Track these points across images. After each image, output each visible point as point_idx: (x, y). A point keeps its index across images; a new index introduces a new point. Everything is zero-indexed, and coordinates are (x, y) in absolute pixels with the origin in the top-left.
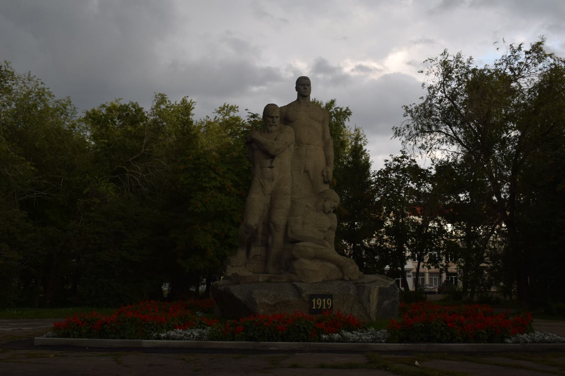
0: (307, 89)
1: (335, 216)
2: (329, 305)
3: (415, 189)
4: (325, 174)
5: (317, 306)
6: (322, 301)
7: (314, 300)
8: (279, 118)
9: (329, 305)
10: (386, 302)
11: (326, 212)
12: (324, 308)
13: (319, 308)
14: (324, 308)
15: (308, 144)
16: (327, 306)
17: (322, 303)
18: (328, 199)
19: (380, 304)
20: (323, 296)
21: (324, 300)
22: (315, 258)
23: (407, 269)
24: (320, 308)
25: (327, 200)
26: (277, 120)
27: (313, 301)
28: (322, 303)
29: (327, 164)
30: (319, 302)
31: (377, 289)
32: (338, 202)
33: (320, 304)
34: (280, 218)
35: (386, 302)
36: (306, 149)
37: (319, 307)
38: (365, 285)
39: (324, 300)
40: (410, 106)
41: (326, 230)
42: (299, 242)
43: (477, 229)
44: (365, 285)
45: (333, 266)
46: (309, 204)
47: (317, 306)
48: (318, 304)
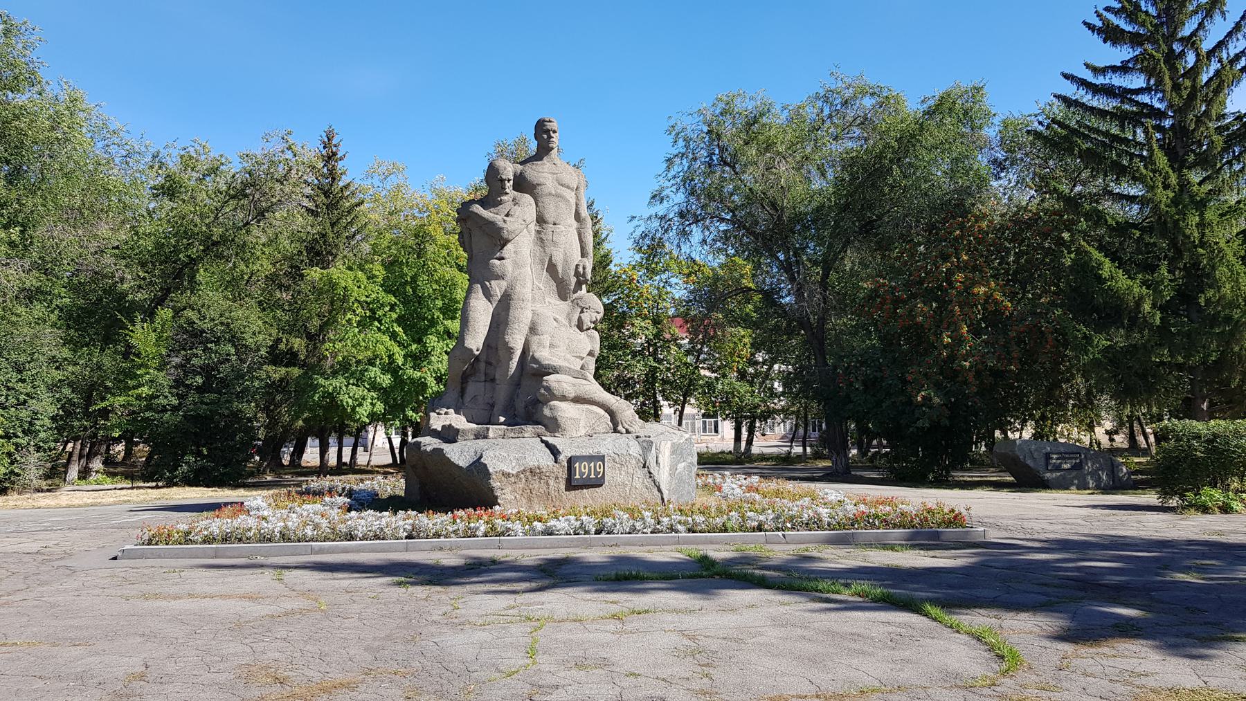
1: (596, 334)
4: (581, 270)
5: (581, 474)
7: (577, 465)
8: (511, 182)
10: (681, 466)
11: (585, 328)
12: (593, 476)
14: (593, 476)
15: (555, 224)
16: (597, 473)
17: (590, 468)
19: (673, 468)
20: (590, 458)
21: (592, 464)
22: (578, 400)
23: (559, 414)
25: (585, 310)
26: (509, 185)
28: (590, 468)
29: (584, 254)
34: (516, 341)
35: (681, 466)
38: (651, 439)
39: (592, 464)
40: (20, 384)
41: (585, 356)
42: (550, 374)
43: (120, 447)
44: (651, 439)
45: (602, 412)
48: (598, 470)
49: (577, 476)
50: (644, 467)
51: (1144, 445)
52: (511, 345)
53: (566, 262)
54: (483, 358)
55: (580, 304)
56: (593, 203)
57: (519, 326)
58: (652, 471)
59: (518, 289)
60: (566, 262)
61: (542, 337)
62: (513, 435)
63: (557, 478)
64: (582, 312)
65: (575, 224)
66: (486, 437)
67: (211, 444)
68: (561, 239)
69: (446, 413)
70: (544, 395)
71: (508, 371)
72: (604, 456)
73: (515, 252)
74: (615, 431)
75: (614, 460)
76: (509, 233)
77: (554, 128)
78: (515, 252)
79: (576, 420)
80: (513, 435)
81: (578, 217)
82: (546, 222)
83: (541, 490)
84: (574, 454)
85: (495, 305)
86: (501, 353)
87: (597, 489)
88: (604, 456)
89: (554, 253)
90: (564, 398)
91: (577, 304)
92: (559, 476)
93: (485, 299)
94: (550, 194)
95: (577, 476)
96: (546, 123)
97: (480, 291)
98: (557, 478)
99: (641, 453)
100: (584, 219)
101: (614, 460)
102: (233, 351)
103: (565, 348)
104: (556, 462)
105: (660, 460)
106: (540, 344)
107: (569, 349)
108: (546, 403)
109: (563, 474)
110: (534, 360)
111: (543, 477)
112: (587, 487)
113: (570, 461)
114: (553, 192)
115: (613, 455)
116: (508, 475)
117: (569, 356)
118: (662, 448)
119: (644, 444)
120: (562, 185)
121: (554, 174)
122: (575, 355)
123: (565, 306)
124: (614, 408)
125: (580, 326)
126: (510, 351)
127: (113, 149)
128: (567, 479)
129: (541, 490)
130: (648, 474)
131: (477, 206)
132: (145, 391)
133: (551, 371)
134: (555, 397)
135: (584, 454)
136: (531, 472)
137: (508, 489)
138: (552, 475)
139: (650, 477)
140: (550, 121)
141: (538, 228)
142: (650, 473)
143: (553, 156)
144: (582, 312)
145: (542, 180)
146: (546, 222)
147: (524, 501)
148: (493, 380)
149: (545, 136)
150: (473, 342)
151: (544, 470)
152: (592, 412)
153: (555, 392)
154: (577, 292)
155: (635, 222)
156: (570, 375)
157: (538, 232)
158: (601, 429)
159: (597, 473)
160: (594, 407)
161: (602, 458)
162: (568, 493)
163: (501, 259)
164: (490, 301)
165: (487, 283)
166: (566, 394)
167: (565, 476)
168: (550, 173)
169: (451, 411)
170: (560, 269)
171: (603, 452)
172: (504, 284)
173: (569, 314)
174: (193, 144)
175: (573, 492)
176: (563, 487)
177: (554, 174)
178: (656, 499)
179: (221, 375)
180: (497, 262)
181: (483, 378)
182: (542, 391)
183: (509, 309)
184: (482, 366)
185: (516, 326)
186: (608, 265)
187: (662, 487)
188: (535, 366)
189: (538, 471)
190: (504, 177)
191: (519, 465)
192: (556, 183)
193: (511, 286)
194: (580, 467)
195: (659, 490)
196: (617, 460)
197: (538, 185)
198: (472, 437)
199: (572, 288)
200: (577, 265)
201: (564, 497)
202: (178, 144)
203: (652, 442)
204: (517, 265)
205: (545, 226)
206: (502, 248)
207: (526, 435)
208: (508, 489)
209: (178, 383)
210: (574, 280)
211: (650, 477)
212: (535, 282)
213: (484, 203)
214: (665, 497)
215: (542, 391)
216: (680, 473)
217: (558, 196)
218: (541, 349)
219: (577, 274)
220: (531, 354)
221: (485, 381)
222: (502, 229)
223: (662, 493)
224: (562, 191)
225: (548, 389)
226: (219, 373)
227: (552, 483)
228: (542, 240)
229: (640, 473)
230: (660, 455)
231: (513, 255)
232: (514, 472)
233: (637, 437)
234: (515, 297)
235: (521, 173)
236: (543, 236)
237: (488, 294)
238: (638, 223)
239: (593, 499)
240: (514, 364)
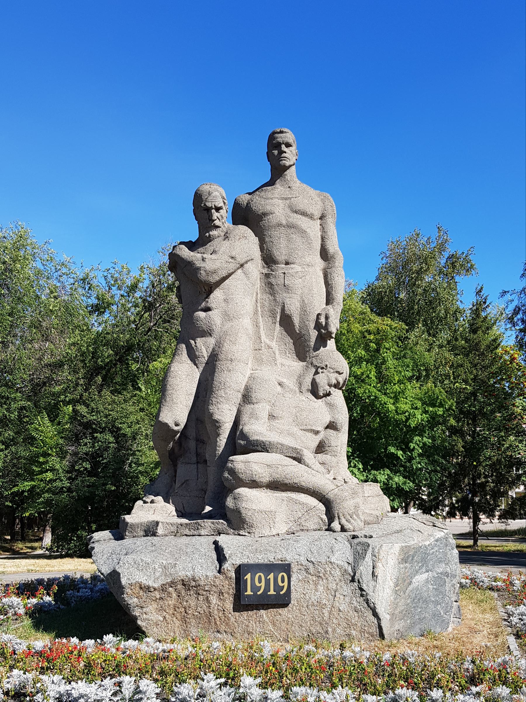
0: (285, 152)
2: (284, 586)
3: (208, 232)
4: (323, 320)
5: (255, 589)
6: (266, 579)
7: (248, 576)
9: (284, 586)
12: (272, 592)
13: (282, 593)
14: (272, 592)
15: (287, 263)
16: (278, 588)
17: (268, 582)
18: (322, 368)
21: (271, 576)
23: (243, 505)
24: (260, 594)
25: (320, 370)
27: (245, 578)
28: (268, 582)
29: (329, 300)
30: (260, 582)
31: (397, 547)
32: (345, 374)
33: (263, 584)
35: (420, 579)
36: (284, 273)
37: (259, 591)
39: (271, 576)
46: (285, 380)
47: (255, 589)
48: (281, 584)
49: (249, 592)
50: (353, 580)
51: (206, 287)
52: (216, 417)
53: (304, 311)
54: (192, 433)
55: (315, 363)
56: (482, 288)
57: (226, 393)
58: (365, 587)
59: (227, 346)
60: (304, 311)
61: (256, 406)
62: (187, 532)
63: (221, 593)
64: (317, 373)
65: (320, 264)
66: (154, 534)
67: (100, 521)
68: (295, 282)
69: (152, 502)
70: (227, 479)
71: (216, 450)
72: (289, 565)
73: (226, 300)
74: (329, 529)
75: (307, 570)
76: (207, 274)
77: (286, 140)
78: (226, 300)
79: (270, 514)
80: (187, 532)
81: (325, 254)
82: (275, 262)
83: (199, 609)
84: (245, 561)
85: (201, 369)
86: (209, 427)
87: (280, 610)
88: (289, 565)
89: (287, 301)
90: (254, 484)
91: (312, 364)
92: (225, 589)
93: (189, 362)
94: (280, 225)
95: (249, 592)
96: (277, 135)
97: (185, 352)
98: (221, 593)
99: (351, 560)
100: (333, 257)
101: (307, 570)
102: (112, 439)
103: (291, 420)
104: (219, 572)
105: (379, 571)
106: (253, 415)
107: (296, 421)
108: (230, 490)
109: (229, 588)
110: (244, 436)
111: (201, 592)
112: (266, 606)
113: (240, 570)
114: (284, 222)
115: (305, 563)
116: (147, 589)
117: (295, 429)
118: (382, 554)
119: (358, 548)
120: (296, 212)
121: (286, 199)
122: (304, 427)
123: (298, 365)
124: (331, 496)
125: (314, 391)
126: (216, 425)
127: (64, 278)
128: (235, 595)
129: (199, 609)
130: (358, 591)
131: (184, 246)
132: (49, 475)
133: (259, 448)
134: (242, 483)
135: (261, 562)
136: (184, 585)
137: (151, 608)
138: (214, 589)
139: (362, 595)
140: (281, 132)
141: (265, 271)
142: (361, 589)
143: (288, 177)
144: (317, 373)
145: (268, 208)
146: (275, 262)
147: (178, 623)
148: (205, 461)
149: (276, 152)
150: (170, 414)
151: (202, 583)
152: (296, 502)
153: (241, 476)
154: (318, 349)
155: (508, 297)
156: (282, 453)
157: (267, 276)
158: (311, 524)
159: (278, 588)
160: (303, 495)
161: (286, 568)
162: (237, 614)
163: (207, 309)
164: (195, 364)
165: (192, 342)
166: (257, 478)
167: (232, 591)
168: (282, 199)
169: (160, 498)
170: (296, 321)
171: (289, 557)
172: (211, 341)
173: (300, 377)
174: (114, 266)
175: (245, 614)
176: (229, 605)
177: (286, 199)
178: (370, 626)
179: (105, 461)
180: (201, 314)
181: (194, 459)
182: (226, 475)
183: (214, 372)
184: (192, 444)
185: (222, 393)
186: (496, 348)
187: (380, 610)
188: (242, 442)
189: (193, 584)
190: (209, 204)
191: (166, 575)
192: (288, 211)
193: (219, 345)
194: (253, 579)
195: (375, 614)
196: (312, 570)
197: (265, 214)
198: (142, 533)
199: (312, 344)
200: (319, 315)
201: (233, 619)
202: (103, 267)
203: (369, 545)
204: (227, 317)
205: (274, 267)
206: (208, 296)
207: (203, 532)
208: (151, 608)
209: (71, 469)
210: (314, 334)
211: (362, 595)
212: (263, 337)
213: (192, 246)
214: (383, 625)
215: (226, 475)
216: (417, 589)
217: (290, 226)
218: (253, 421)
219: (318, 326)
220: (241, 427)
221: (198, 463)
222: (199, 269)
223: (379, 619)
224: (302, 222)
225: (233, 472)
226: (103, 460)
227: (214, 599)
228: (270, 285)
229: (347, 589)
230: (379, 565)
231: (223, 304)
232: (156, 585)
233: (354, 537)
234: (222, 356)
235: (247, 204)
236: (273, 280)
237: (193, 356)
238: (510, 298)
239: (274, 625)
240: (222, 441)
